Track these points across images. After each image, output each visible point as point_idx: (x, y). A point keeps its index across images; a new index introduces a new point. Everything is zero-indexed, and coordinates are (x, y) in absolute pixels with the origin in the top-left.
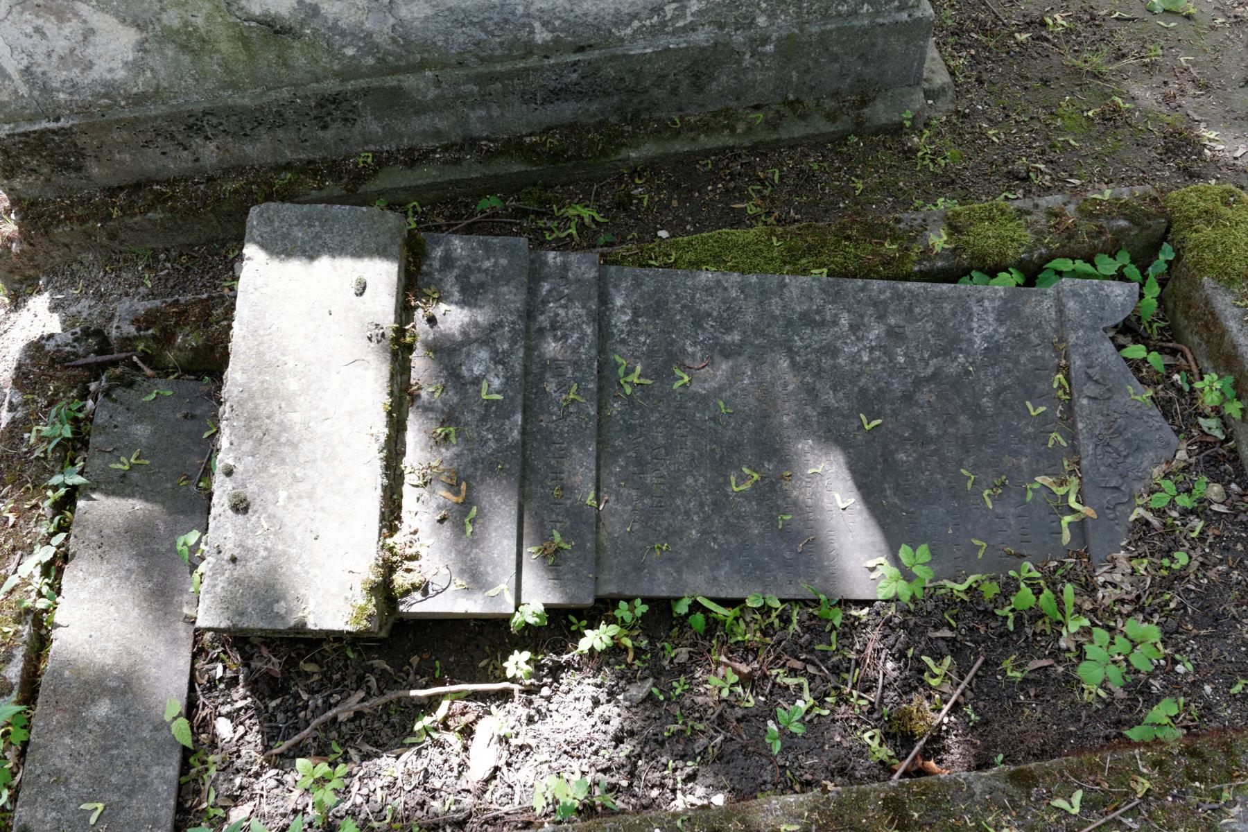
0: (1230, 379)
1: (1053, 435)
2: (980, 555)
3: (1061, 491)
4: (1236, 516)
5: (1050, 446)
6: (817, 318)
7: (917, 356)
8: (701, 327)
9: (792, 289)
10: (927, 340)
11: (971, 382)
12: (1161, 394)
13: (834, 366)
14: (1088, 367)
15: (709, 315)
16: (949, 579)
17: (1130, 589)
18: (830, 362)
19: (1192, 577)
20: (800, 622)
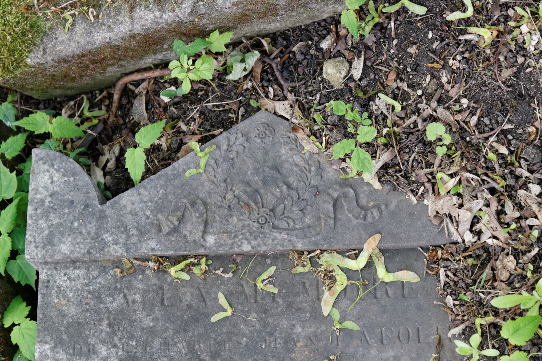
0: (178, 44)
1: (260, 285)
3: (342, 280)
4: (368, 48)
5: (276, 291)
12: (194, 126)
14: (160, 231)
17: (481, 202)
19: (459, 117)
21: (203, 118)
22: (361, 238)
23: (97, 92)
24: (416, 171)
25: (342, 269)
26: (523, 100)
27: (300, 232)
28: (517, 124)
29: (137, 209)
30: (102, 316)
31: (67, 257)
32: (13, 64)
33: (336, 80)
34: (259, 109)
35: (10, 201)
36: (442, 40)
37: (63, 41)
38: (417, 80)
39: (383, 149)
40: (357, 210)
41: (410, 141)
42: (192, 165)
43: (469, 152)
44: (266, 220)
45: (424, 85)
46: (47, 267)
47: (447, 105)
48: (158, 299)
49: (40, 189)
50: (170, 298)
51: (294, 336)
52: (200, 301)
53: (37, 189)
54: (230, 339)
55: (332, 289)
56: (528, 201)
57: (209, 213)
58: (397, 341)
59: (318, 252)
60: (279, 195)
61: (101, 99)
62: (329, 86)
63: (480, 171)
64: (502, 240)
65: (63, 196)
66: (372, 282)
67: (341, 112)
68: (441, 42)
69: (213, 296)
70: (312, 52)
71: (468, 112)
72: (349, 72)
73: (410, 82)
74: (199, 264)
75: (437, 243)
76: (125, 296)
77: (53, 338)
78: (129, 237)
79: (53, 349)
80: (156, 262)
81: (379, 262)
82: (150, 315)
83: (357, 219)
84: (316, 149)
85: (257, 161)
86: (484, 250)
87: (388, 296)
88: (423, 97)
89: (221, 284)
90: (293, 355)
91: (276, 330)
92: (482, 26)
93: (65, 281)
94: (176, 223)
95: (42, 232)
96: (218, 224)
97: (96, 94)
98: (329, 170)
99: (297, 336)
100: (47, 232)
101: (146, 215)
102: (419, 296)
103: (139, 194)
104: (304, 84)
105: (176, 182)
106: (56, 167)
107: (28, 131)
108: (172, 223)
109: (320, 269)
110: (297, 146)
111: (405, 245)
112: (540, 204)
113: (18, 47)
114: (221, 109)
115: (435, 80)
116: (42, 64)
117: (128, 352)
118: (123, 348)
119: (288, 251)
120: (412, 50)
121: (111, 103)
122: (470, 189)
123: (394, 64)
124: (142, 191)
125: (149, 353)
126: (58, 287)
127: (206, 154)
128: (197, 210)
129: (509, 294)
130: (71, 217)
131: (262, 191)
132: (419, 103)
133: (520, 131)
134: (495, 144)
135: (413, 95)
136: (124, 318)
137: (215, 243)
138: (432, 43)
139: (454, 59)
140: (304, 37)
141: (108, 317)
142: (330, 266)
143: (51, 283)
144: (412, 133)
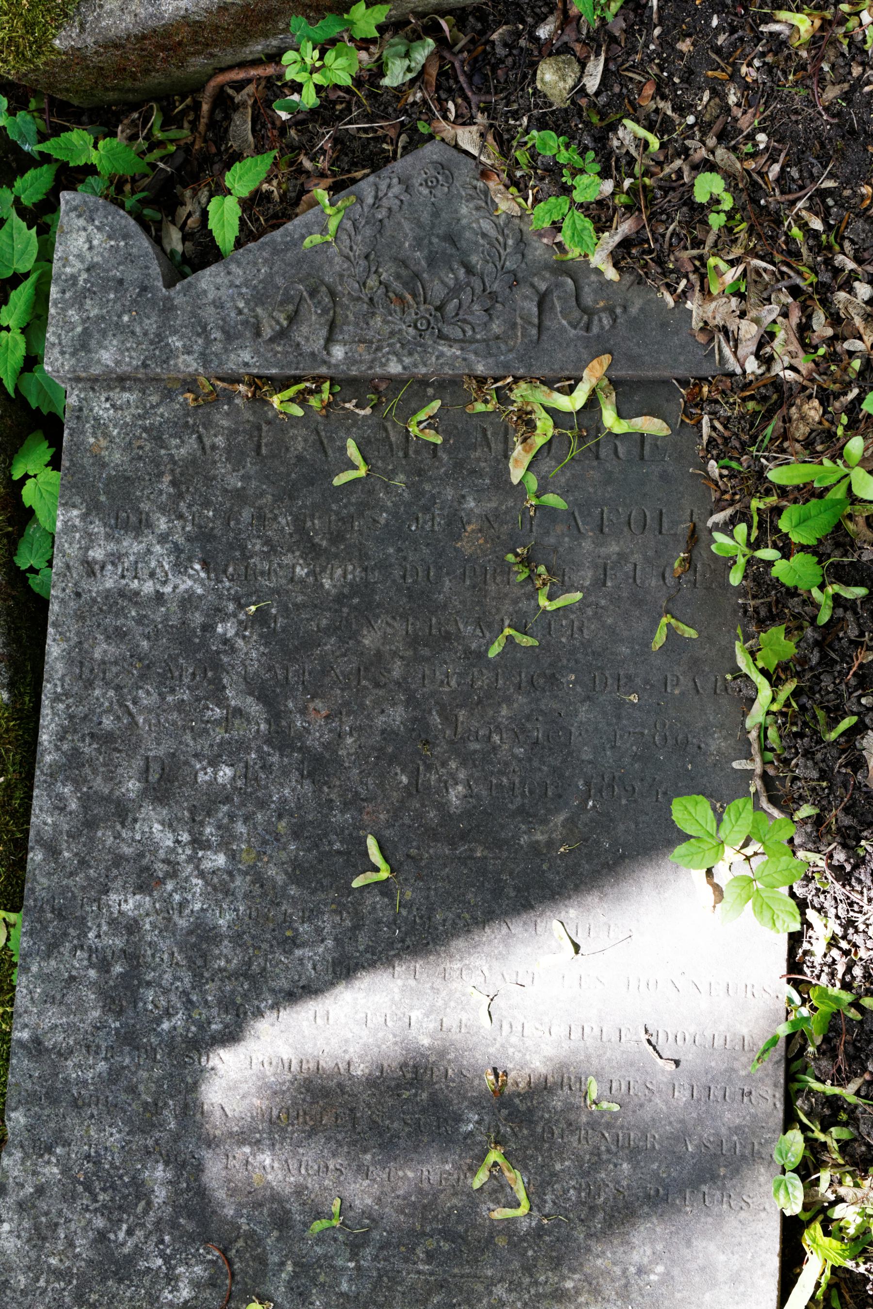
0: (298, 23)
1: (414, 430)
2: (690, 633)
3: (545, 427)
4: (613, 40)
5: (439, 440)
6: (118, 969)
7: (219, 735)
8: (130, 1260)
9: (46, 1024)
10: (180, 706)
11: (284, 610)
12: (323, 163)
13: (237, 939)
14: (258, 334)
15: (102, 1236)
16: (745, 715)
17: (776, 309)
18: (226, 947)
19: (751, 165)
20: (840, 1082)
21: (340, 151)
22: (580, 360)
23: (176, 97)
24: (677, 253)
25: (549, 410)
26: (855, 140)
27: (481, 347)
28: (843, 179)
29: (224, 298)
30: (162, 468)
31: (109, 371)
32: (31, 48)
33: (557, 92)
34: (431, 137)
35: (26, 275)
36: (733, 30)
37: (112, 11)
38: (688, 98)
39: (624, 214)
40: (576, 314)
41: (669, 201)
42: (316, 228)
43: (761, 225)
44: (429, 323)
45: (699, 108)
46: (80, 386)
47: (733, 143)
48: (251, 445)
49: (71, 258)
50: (271, 444)
51: (463, 514)
52: (317, 451)
53: (67, 259)
54: (361, 514)
55: (529, 441)
56: (850, 309)
57: (338, 310)
58: (626, 529)
59: (510, 380)
60: (451, 283)
61: (183, 110)
62: (545, 103)
63: (778, 258)
64: (804, 372)
65: (108, 271)
66: (593, 432)
67: (550, 150)
68: (731, 34)
69: (338, 443)
70: (522, 43)
71: (767, 155)
72: (580, 80)
73: (678, 101)
74: (318, 391)
75: (702, 373)
76: (200, 438)
77: (84, 500)
78: (208, 342)
79: (84, 517)
80: (250, 385)
81: (607, 401)
82: (238, 471)
83: (575, 328)
84: (517, 208)
85: (420, 225)
86: (775, 388)
87: (618, 457)
88: (696, 129)
89: (353, 425)
90: (459, 545)
91: (435, 503)
92: (799, 10)
93: (107, 409)
94: (285, 323)
95: (73, 330)
96: (351, 328)
97: (174, 101)
98: (537, 245)
99: (468, 515)
100: (79, 329)
101: (237, 308)
102: (667, 459)
103: (229, 273)
104: (506, 98)
105: (289, 255)
106: (97, 223)
107: (57, 160)
108: (278, 322)
109: (511, 408)
110: (486, 203)
111: (651, 374)
112: (869, 315)
113: (41, 19)
114: (371, 135)
115: (717, 100)
116: (79, 49)
117: (200, 527)
118: (193, 519)
119: (461, 376)
120: (685, 46)
121: (198, 117)
122: (760, 287)
123: (653, 70)
124: (233, 267)
125: (233, 530)
126: (95, 419)
127: (339, 211)
128: (319, 303)
129: (805, 462)
130: (118, 306)
131: (425, 275)
132: (688, 137)
133: (847, 193)
134: (804, 213)
135: (680, 124)
136: (197, 473)
137: (345, 359)
138: (716, 37)
139: (750, 65)
140: (512, 17)
141: (172, 471)
142: (528, 403)
143: (85, 412)
144: (674, 189)
